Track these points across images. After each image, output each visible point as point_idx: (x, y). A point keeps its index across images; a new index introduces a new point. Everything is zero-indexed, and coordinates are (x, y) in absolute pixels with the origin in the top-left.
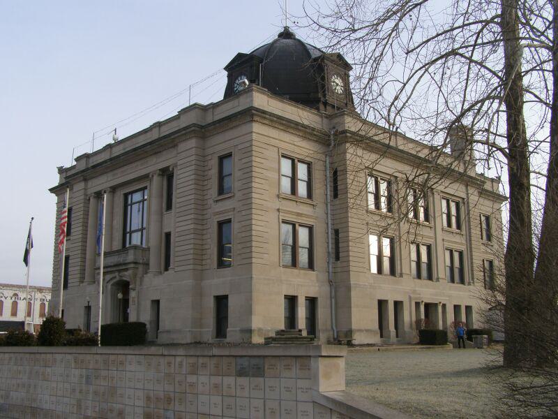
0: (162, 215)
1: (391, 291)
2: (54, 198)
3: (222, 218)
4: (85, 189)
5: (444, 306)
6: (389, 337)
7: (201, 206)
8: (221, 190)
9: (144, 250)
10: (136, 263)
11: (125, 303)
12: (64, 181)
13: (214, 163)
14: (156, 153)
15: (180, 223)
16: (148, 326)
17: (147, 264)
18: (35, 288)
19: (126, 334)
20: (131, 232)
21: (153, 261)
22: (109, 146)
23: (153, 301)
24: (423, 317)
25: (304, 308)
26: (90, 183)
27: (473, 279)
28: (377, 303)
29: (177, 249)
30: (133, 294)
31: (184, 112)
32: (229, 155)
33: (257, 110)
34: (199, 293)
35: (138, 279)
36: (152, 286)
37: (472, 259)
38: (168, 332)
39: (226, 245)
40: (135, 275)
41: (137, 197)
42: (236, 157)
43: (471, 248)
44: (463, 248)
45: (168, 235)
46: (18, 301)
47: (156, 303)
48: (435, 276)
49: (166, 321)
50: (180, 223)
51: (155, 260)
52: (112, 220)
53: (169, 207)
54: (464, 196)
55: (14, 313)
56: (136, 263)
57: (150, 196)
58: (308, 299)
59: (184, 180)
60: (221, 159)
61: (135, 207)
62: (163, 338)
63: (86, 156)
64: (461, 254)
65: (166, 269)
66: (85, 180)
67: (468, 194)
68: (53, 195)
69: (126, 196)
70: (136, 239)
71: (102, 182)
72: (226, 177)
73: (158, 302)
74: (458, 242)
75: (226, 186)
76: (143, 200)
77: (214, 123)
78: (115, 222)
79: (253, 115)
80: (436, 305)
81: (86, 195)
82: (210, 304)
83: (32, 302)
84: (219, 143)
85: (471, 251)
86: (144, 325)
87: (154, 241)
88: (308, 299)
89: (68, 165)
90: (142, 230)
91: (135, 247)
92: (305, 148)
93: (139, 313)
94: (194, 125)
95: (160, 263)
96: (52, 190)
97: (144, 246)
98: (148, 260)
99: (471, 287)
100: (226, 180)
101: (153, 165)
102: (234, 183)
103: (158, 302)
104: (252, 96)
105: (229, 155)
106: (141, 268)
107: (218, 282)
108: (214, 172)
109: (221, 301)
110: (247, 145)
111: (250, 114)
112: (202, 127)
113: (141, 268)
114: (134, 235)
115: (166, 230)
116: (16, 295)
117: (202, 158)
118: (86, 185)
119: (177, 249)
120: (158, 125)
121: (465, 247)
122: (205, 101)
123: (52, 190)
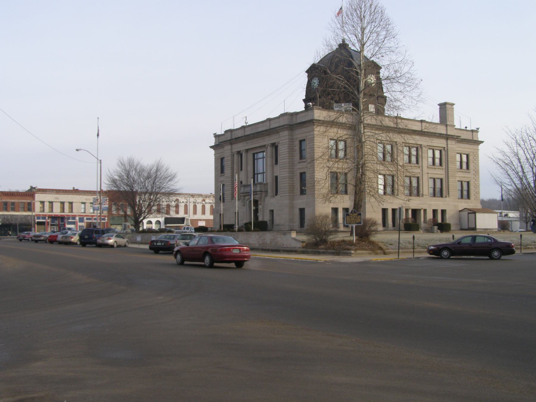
0: (273, 167)
1: (391, 203)
2: (212, 151)
3: (302, 171)
4: (231, 149)
5: (425, 211)
6: (388, 227)
7: (292, 165)
8: (301, 157)
9: (265, 184)
10: (261, 191)
11: (256, 211)
12: (217, 143)
13: (297, 143)
14: (269, 135)
15: (282, 172)
16: (268, 222)
17: (266, 192)
18: (189, 194)
19: (261, 226)
20: (257, 174)
21: (269, 191)
22: (243, 127)
23: (270, 210)
24: (410, 216)
25: (342, 214)
26: (234, 146)
27: (449, 194)
28: (381, 210)
29: (281, 185)
30: (260, 207)
31: (282, 115)
32: (304, 140)
33: (315, 120)
34: (292, 207)
35: (263, 199)
36: (270, 203)
37: (448, 182)
38: (278, 225)
39: (304, 184)
40: (261, 198)
41: (261, 155)
42: (307, 142)
43: (448, 176)
44: (443, 176)
45: (276, 177)
46: (179, 204)
47: (272, 211)
48: (421, 193)
49: (277, 220)
50: (282, 172)
51: (270, 189)
52: (247, 167)
53: (276, 163)
54: (445, 146)
55: (177, 212)
56: (261, 191)
57: (266, 154)
58: (344, 209)
59: (283, 150)
60: (301, 142)
61: (260, 161)
62: (275, 228)
63: (231, 131)
64: (441, 180)
65: (276, 195)
66: (231, 144)
67: (447, 145)
68: (212, 150)
69: (254, 154)
70: (260, 178)
71: (241, 147)
72: (303, 150)
73: (273, 211)
74: (439, 173)
75: (303, 155)
76: (263, 158)
77: (296, 124)
78: (249, 168)
79: (314, 123)
80: (420, 210)
81: (232, 152)
82: (297, 212)
83: (188, 204)
84: (299, 134)
85: (448, 178)
86: (266, 222)
87: (269, 180)
88: (344, 209)
89: (219, 133)
90: (263, 173)
91: (260, 183)
92: (342, 133)
93: (264, 216)
94: (286, 125)
95: (273, 156)
96: (211, 147)
97: (265, 182)
98: (267, 189)
99: (447, 199)
100: (303, 152)
101: (268, 141)
102: (307, 153)
103: (273, 211)
104: (313, 112)
105: (304, 140)
106: (264, 194)
107: (301, 202)
108: (297, 148)
109: (302, 211)
110: (312, 136)
111: (312, 122)
112: (291, 125)
113: (264, 194)
114: (259, 176)
115: (276, 175)
116: (177, 200)
117: (292, 140)
118: (231, 147)
119: (281, 185)
120: (269, 120)
121: (444, 176)
122: (291, 110)
123: (211, 147)
